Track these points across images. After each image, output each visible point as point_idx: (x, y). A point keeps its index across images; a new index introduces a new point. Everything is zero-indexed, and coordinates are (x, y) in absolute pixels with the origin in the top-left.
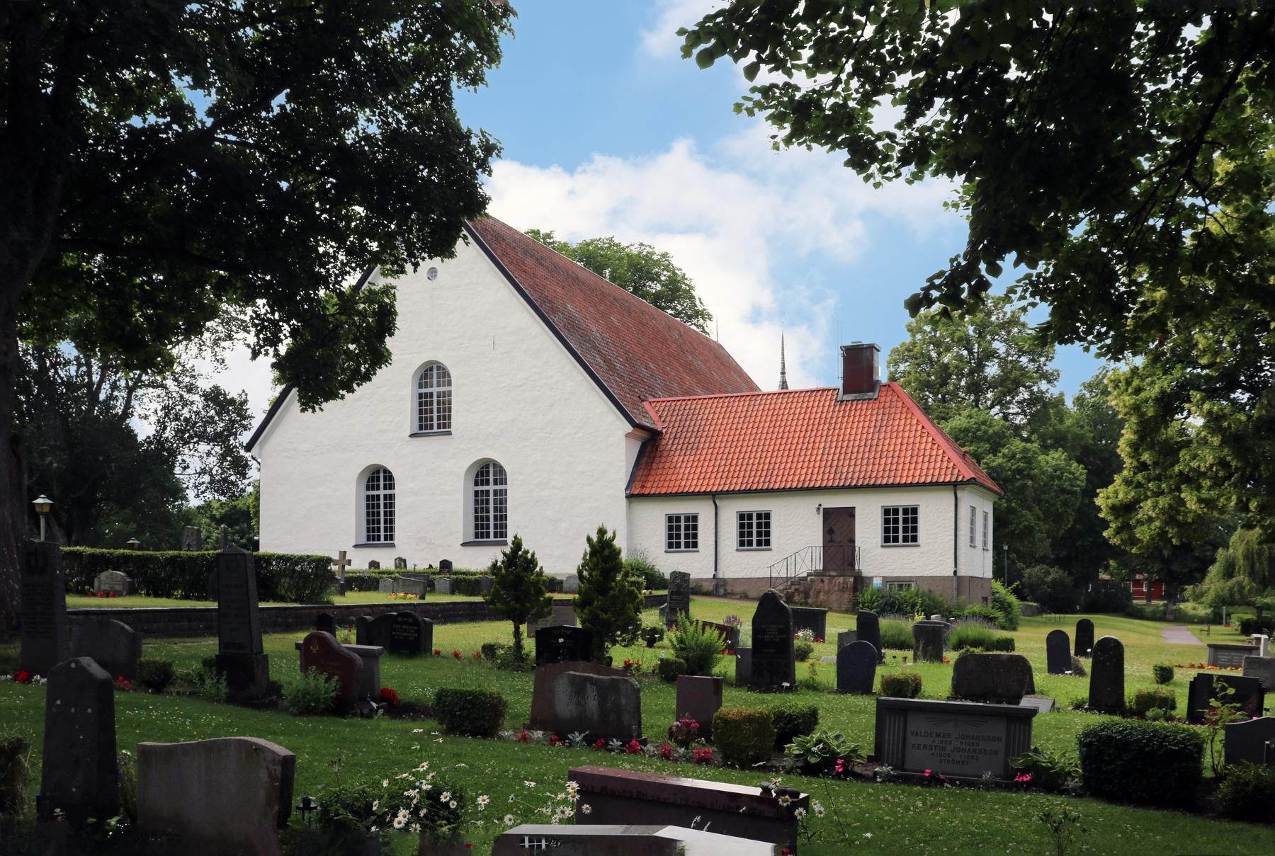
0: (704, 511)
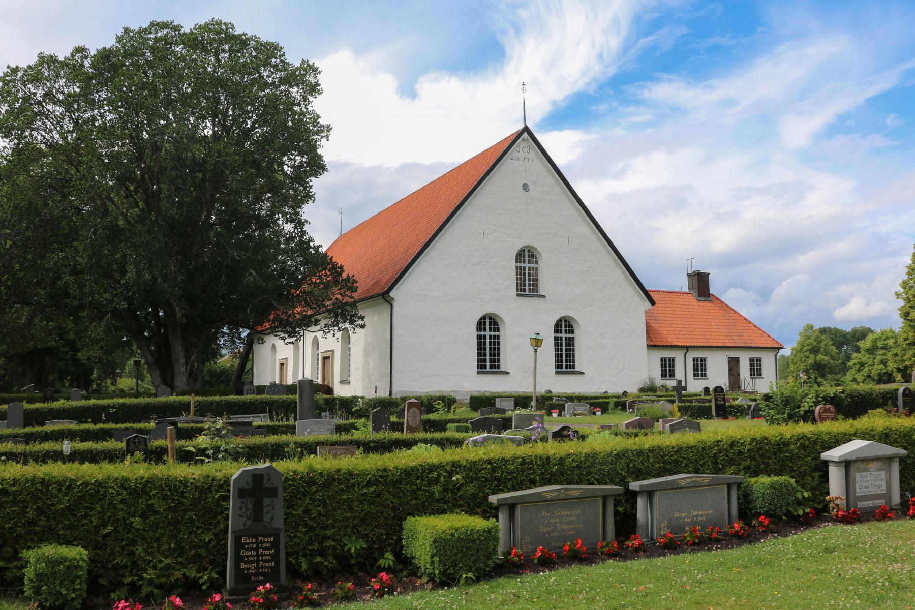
0: (678, 356)
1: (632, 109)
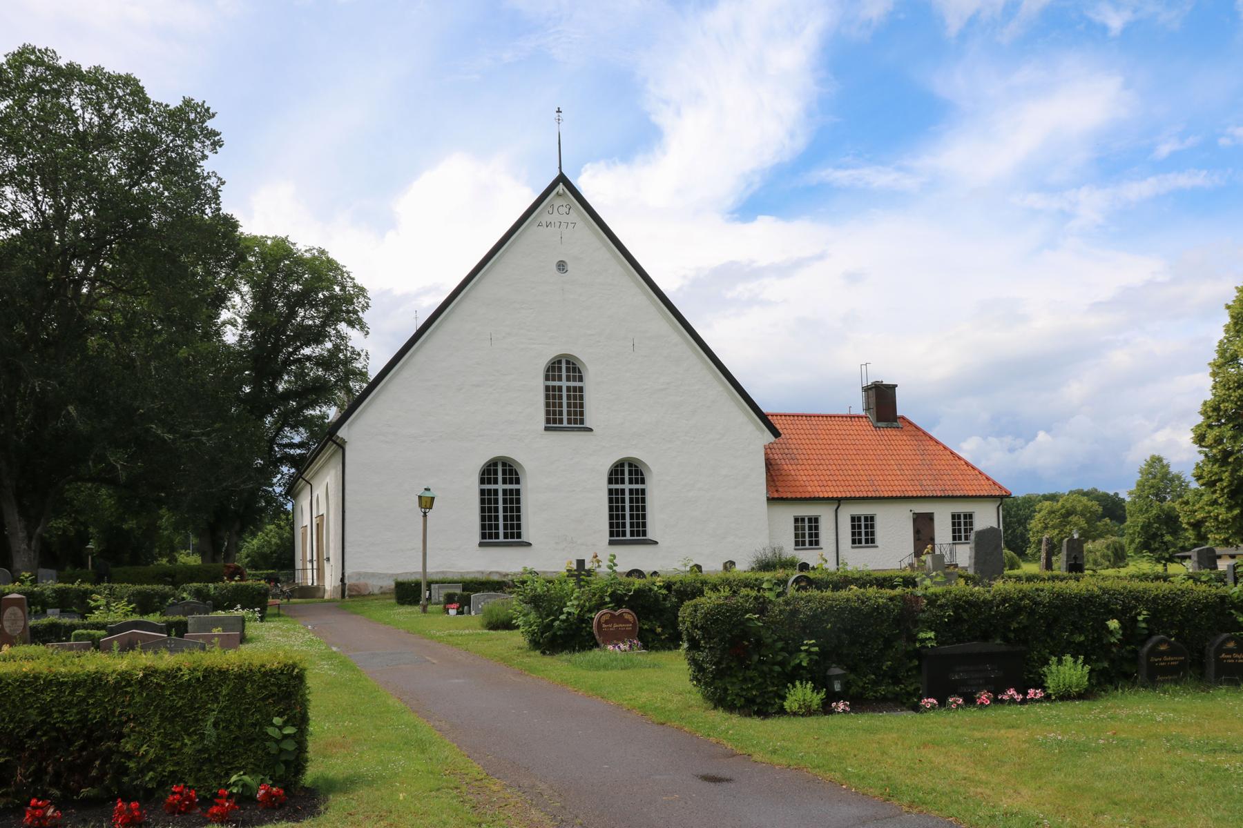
0: (826, 515)
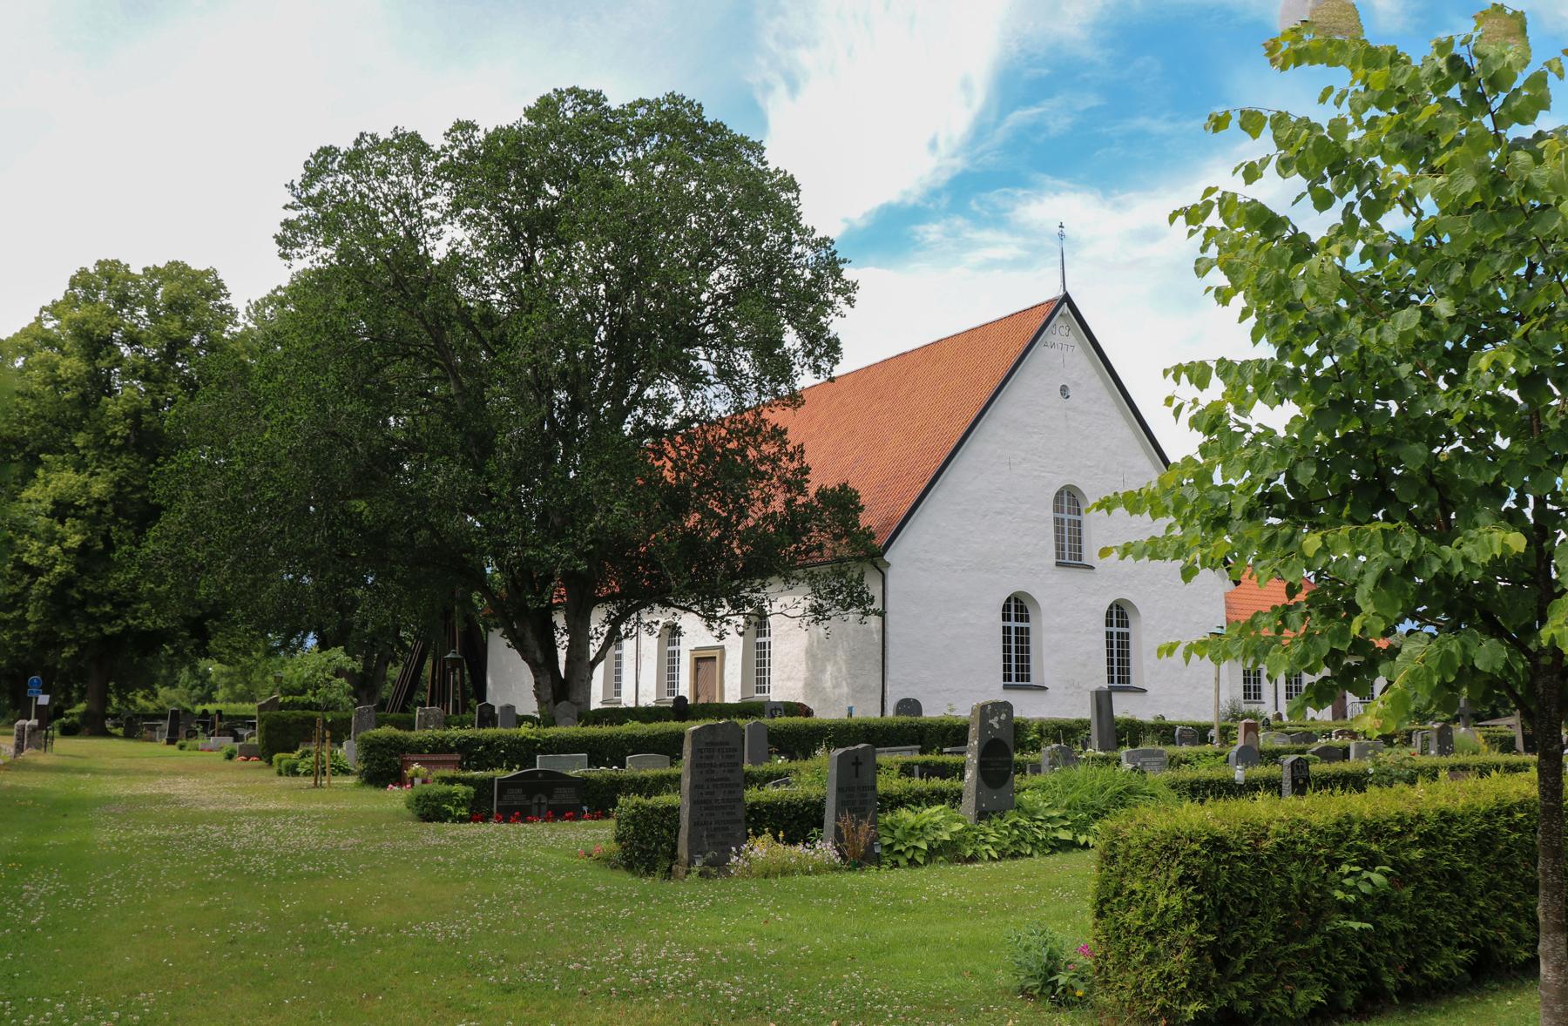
1: (987, 235)
